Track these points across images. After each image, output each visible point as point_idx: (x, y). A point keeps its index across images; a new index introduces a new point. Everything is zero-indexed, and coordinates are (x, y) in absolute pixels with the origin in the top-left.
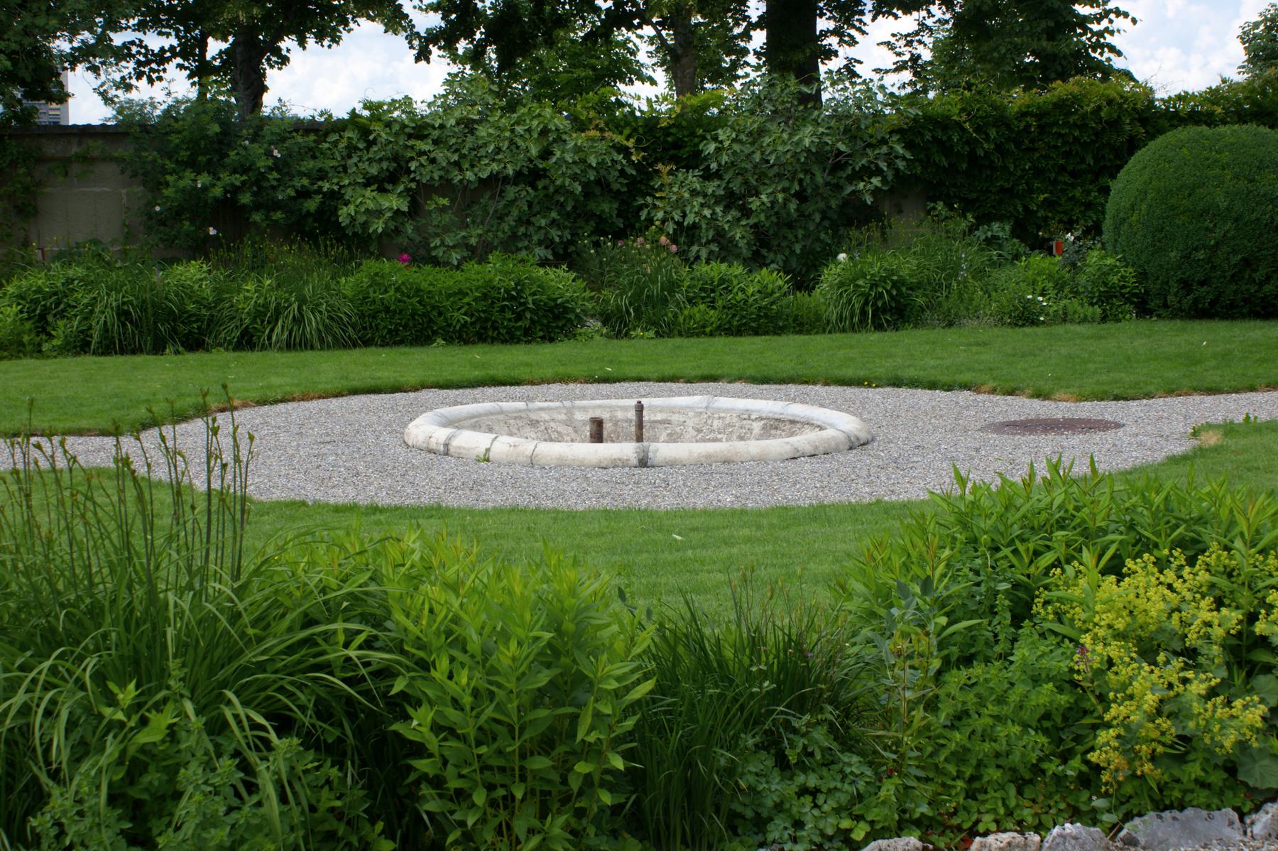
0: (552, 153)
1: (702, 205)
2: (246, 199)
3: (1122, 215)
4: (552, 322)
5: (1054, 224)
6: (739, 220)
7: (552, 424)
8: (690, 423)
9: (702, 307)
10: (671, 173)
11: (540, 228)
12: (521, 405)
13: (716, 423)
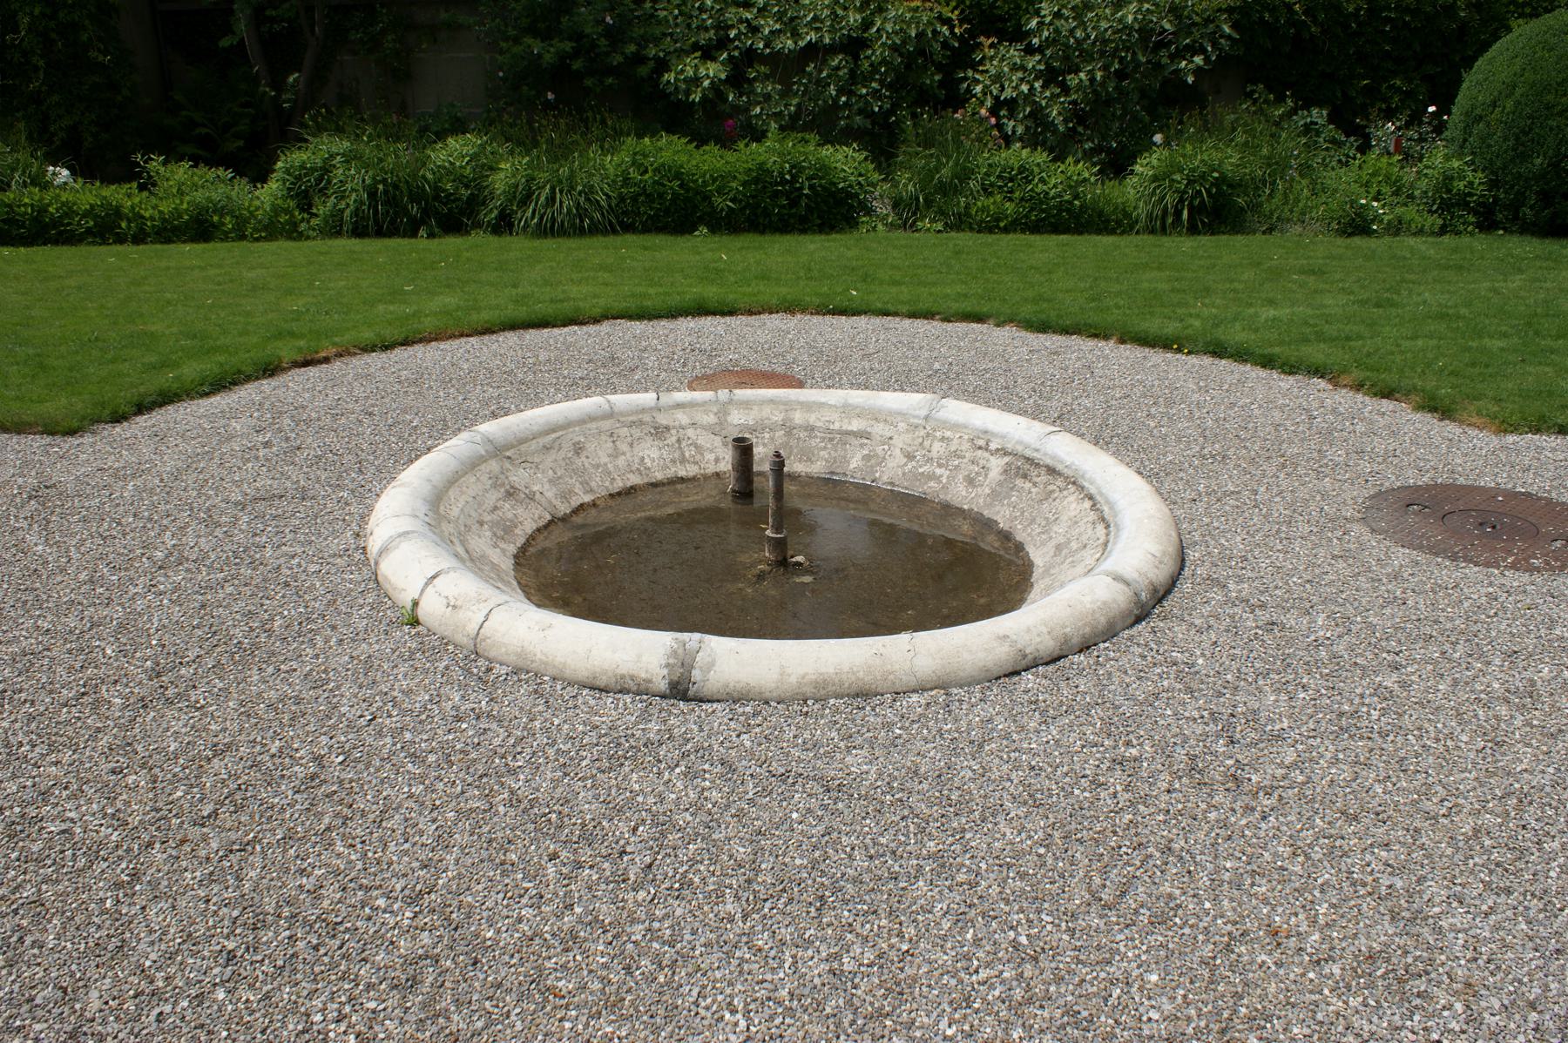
0: (872, 24)
1: (1022, 80)
2: (577, 65)
3: (1478, 111)
4: (832, 210)
5: (1374, 112)
6: (1058, 96)
7: (690, 432)
8: (898, 442)
9: (999, 198)
10: (992, 46)
11: (861, 96)
12: (648, 398)
13: (938, 448)
